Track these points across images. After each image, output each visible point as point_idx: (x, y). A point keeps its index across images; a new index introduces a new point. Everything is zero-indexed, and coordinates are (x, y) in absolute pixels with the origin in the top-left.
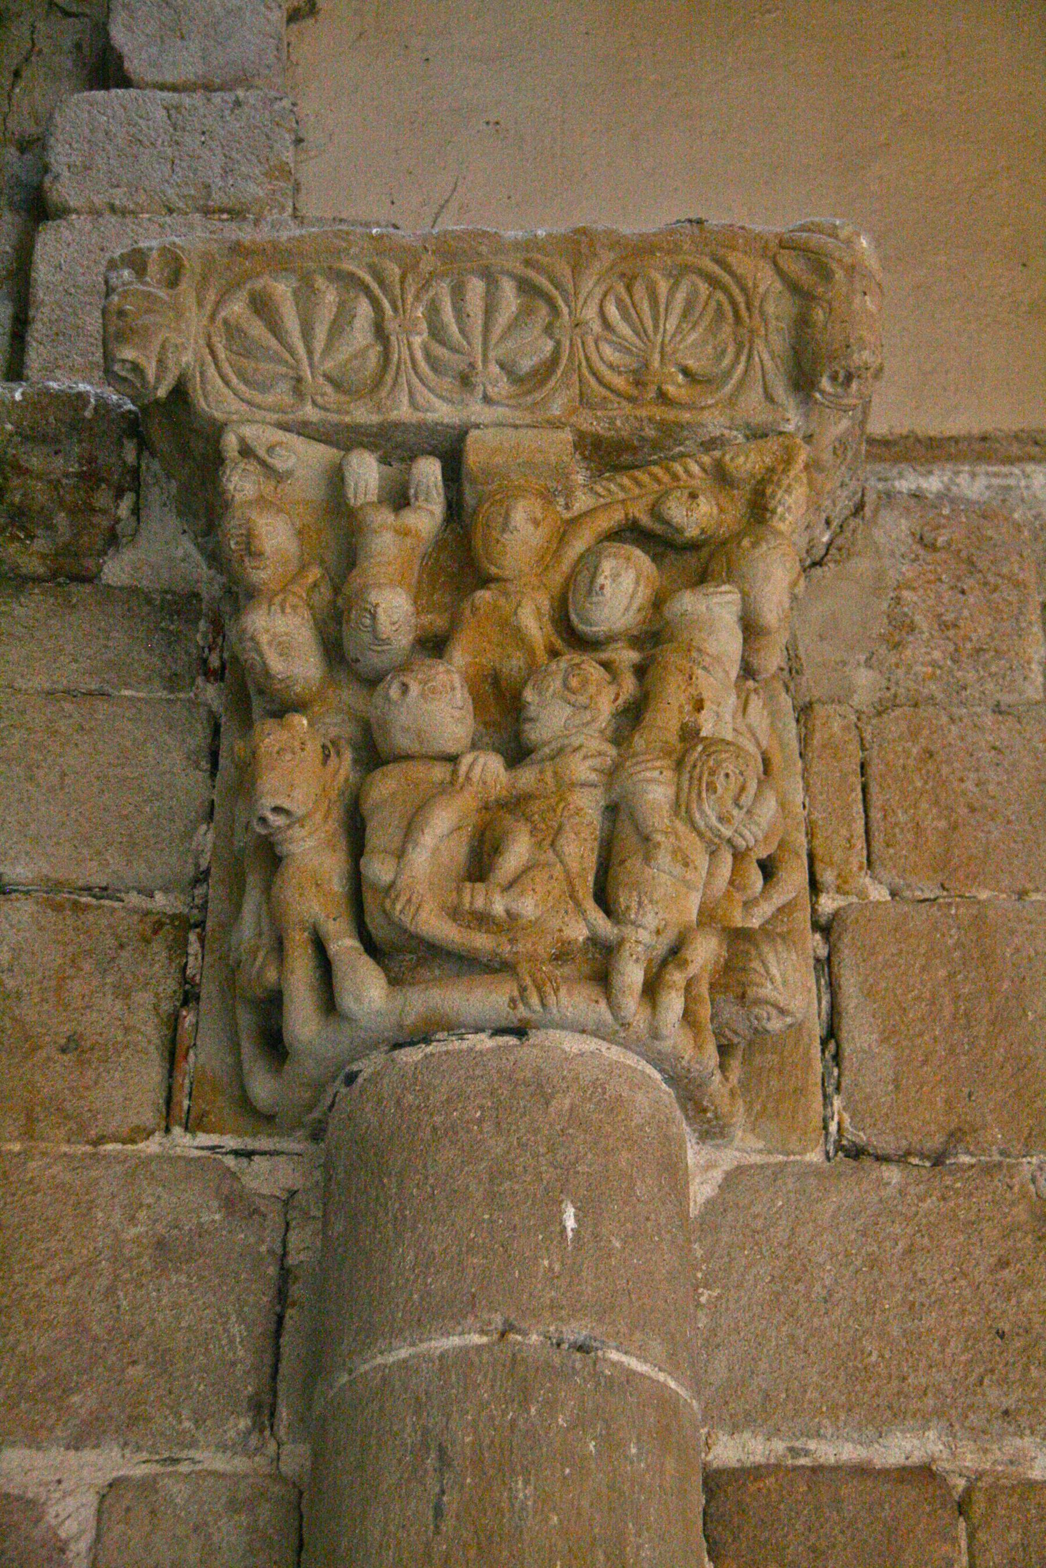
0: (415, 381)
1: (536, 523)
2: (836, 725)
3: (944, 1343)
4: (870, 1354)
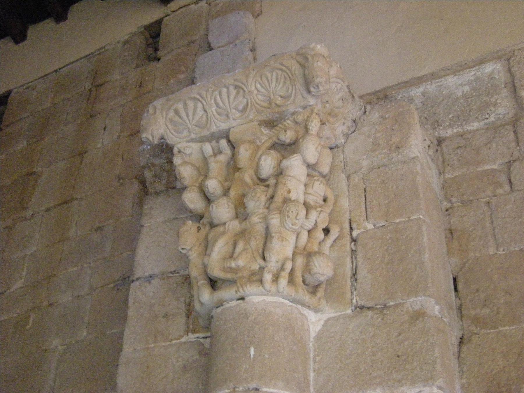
0: (216, 121)
1: (247, 150)
2: (357, 180)
3: (382, 362)
4: (361, 369)
